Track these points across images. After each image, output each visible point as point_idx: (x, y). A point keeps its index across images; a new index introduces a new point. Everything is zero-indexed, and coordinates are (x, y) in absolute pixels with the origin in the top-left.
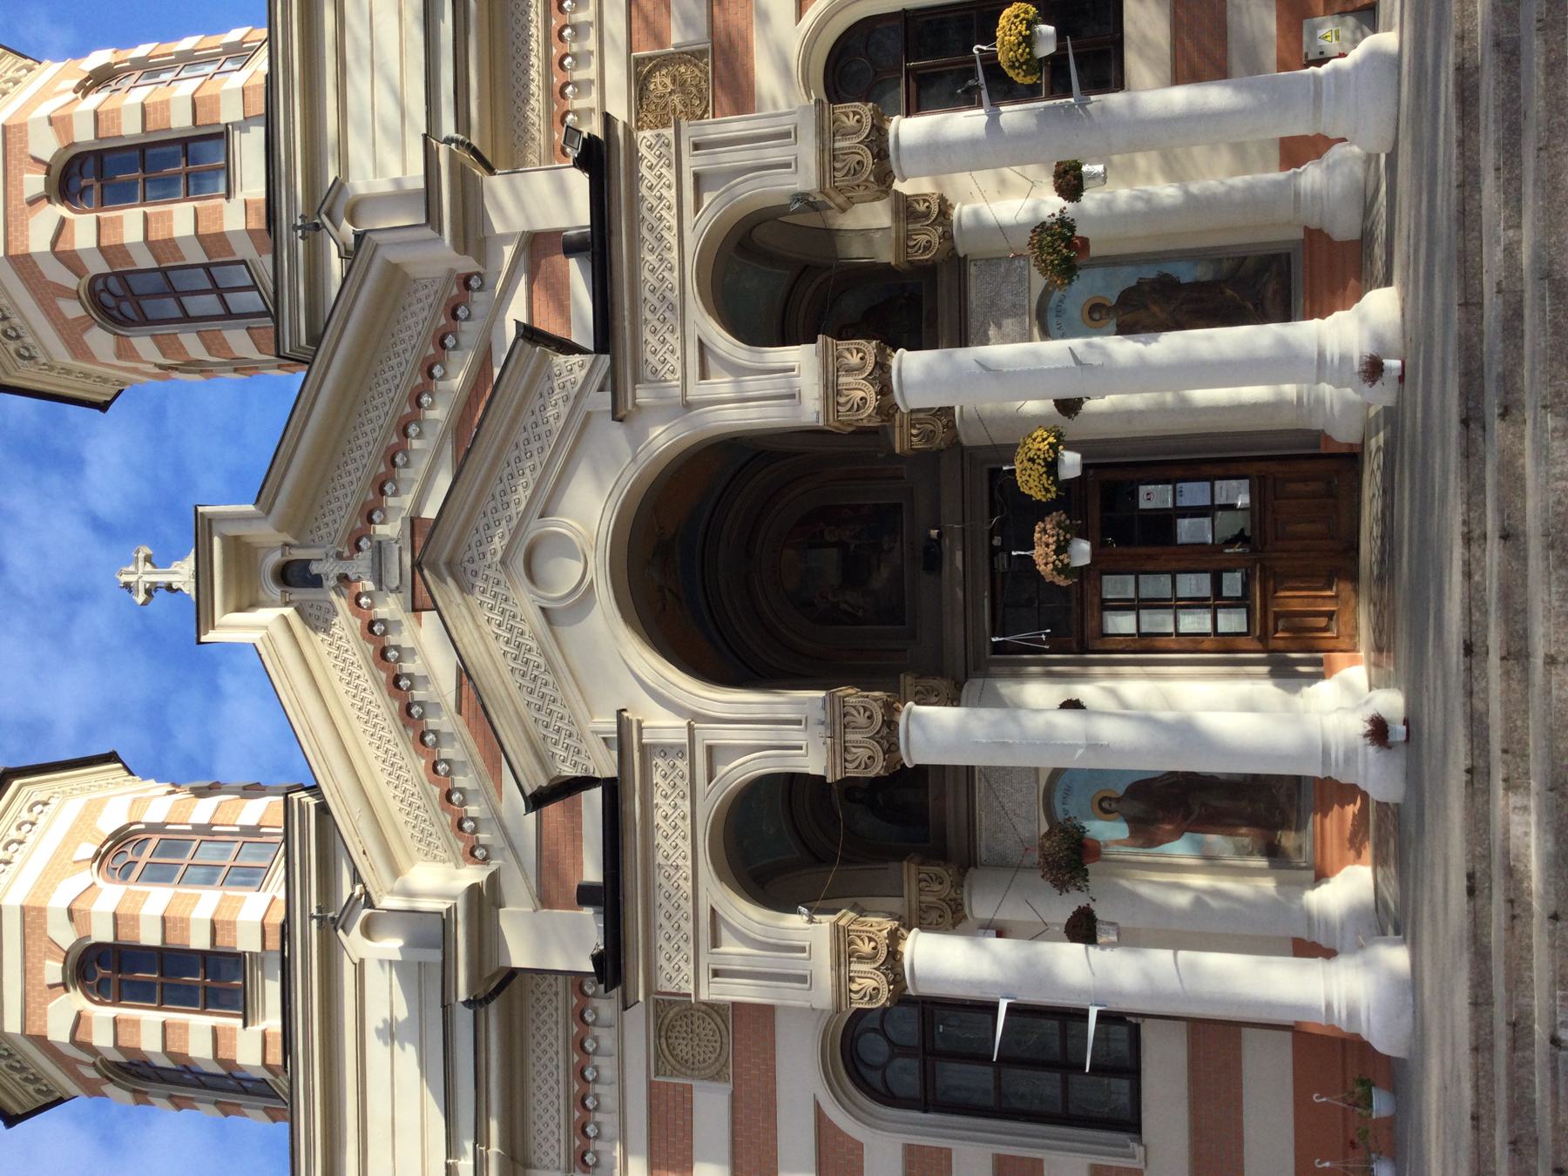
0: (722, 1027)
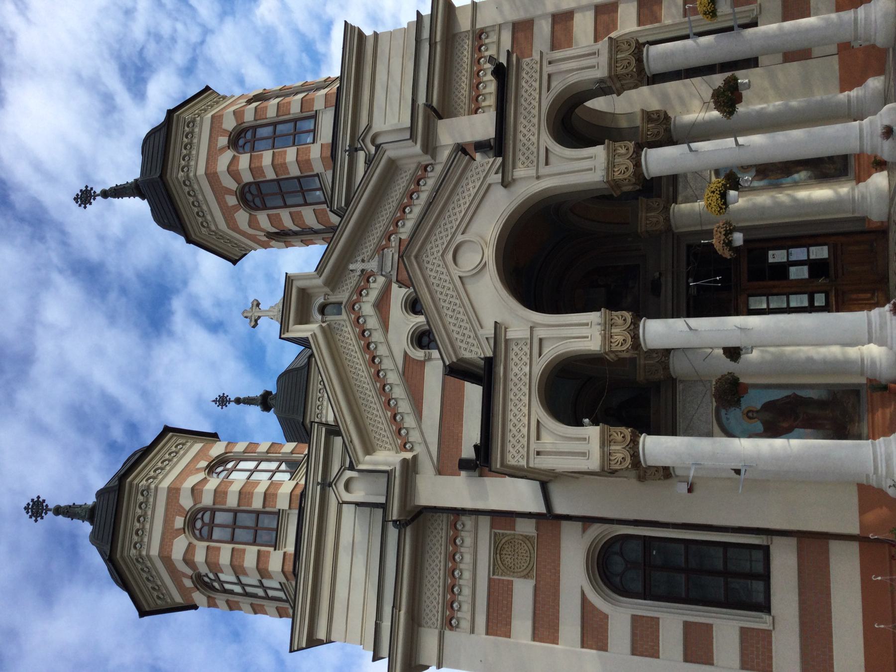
0: (531, 548)
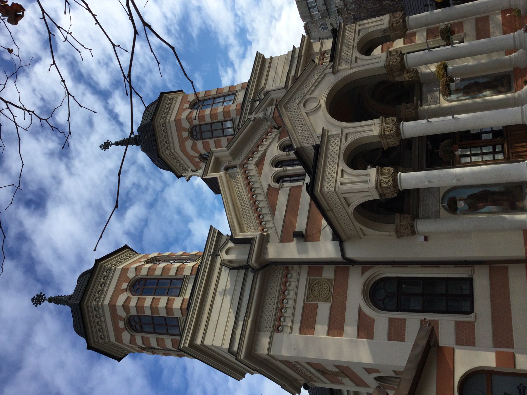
0: (330, 285)
